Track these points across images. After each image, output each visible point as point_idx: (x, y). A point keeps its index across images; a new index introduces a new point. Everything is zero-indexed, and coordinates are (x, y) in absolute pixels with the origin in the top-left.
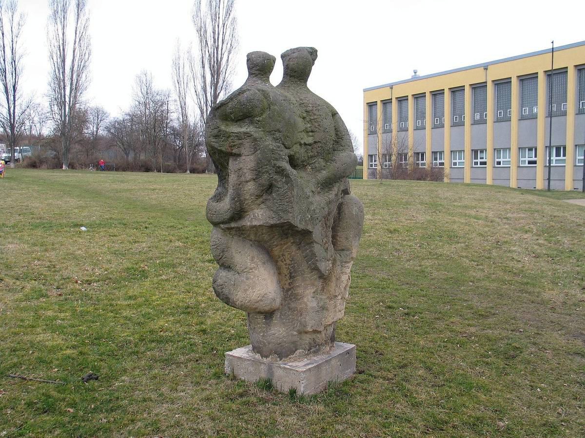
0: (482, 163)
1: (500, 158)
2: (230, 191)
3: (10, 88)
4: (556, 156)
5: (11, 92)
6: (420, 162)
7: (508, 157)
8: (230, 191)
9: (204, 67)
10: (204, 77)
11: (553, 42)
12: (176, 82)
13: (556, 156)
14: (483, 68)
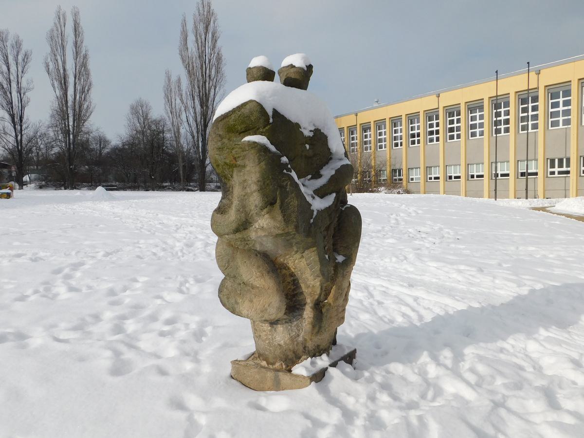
0: (435, 178)
1: (432, 174)
2: (236, 202)
3: (17, 120)
4: (558, 168)
5: (17, 120)
6: (398, 177)
7: (506, 170)
8: (236, 202)
9: (194, 100)
10: (194, 108)
11: (497, 72)
12: (169, 112)
13: (558, 168)
14: (435, 96)
